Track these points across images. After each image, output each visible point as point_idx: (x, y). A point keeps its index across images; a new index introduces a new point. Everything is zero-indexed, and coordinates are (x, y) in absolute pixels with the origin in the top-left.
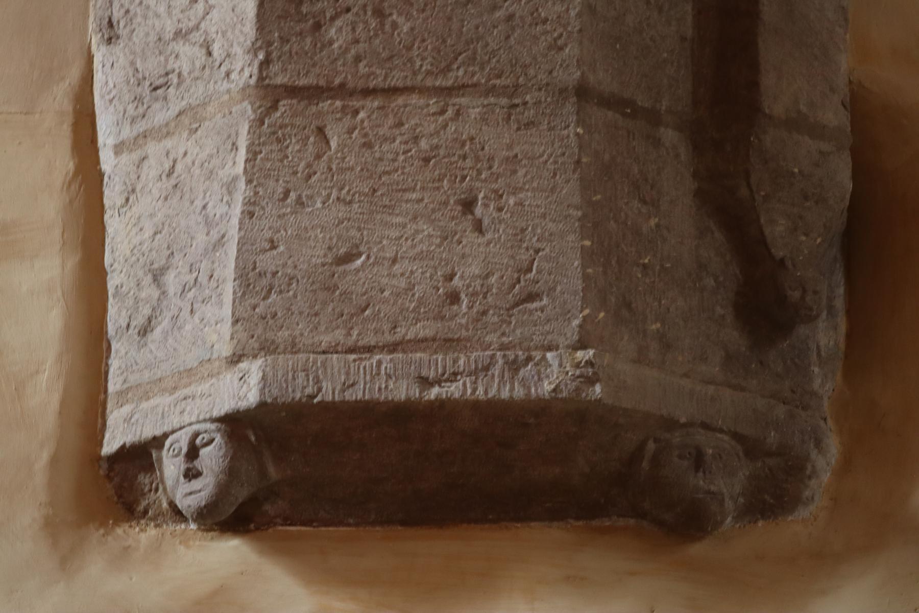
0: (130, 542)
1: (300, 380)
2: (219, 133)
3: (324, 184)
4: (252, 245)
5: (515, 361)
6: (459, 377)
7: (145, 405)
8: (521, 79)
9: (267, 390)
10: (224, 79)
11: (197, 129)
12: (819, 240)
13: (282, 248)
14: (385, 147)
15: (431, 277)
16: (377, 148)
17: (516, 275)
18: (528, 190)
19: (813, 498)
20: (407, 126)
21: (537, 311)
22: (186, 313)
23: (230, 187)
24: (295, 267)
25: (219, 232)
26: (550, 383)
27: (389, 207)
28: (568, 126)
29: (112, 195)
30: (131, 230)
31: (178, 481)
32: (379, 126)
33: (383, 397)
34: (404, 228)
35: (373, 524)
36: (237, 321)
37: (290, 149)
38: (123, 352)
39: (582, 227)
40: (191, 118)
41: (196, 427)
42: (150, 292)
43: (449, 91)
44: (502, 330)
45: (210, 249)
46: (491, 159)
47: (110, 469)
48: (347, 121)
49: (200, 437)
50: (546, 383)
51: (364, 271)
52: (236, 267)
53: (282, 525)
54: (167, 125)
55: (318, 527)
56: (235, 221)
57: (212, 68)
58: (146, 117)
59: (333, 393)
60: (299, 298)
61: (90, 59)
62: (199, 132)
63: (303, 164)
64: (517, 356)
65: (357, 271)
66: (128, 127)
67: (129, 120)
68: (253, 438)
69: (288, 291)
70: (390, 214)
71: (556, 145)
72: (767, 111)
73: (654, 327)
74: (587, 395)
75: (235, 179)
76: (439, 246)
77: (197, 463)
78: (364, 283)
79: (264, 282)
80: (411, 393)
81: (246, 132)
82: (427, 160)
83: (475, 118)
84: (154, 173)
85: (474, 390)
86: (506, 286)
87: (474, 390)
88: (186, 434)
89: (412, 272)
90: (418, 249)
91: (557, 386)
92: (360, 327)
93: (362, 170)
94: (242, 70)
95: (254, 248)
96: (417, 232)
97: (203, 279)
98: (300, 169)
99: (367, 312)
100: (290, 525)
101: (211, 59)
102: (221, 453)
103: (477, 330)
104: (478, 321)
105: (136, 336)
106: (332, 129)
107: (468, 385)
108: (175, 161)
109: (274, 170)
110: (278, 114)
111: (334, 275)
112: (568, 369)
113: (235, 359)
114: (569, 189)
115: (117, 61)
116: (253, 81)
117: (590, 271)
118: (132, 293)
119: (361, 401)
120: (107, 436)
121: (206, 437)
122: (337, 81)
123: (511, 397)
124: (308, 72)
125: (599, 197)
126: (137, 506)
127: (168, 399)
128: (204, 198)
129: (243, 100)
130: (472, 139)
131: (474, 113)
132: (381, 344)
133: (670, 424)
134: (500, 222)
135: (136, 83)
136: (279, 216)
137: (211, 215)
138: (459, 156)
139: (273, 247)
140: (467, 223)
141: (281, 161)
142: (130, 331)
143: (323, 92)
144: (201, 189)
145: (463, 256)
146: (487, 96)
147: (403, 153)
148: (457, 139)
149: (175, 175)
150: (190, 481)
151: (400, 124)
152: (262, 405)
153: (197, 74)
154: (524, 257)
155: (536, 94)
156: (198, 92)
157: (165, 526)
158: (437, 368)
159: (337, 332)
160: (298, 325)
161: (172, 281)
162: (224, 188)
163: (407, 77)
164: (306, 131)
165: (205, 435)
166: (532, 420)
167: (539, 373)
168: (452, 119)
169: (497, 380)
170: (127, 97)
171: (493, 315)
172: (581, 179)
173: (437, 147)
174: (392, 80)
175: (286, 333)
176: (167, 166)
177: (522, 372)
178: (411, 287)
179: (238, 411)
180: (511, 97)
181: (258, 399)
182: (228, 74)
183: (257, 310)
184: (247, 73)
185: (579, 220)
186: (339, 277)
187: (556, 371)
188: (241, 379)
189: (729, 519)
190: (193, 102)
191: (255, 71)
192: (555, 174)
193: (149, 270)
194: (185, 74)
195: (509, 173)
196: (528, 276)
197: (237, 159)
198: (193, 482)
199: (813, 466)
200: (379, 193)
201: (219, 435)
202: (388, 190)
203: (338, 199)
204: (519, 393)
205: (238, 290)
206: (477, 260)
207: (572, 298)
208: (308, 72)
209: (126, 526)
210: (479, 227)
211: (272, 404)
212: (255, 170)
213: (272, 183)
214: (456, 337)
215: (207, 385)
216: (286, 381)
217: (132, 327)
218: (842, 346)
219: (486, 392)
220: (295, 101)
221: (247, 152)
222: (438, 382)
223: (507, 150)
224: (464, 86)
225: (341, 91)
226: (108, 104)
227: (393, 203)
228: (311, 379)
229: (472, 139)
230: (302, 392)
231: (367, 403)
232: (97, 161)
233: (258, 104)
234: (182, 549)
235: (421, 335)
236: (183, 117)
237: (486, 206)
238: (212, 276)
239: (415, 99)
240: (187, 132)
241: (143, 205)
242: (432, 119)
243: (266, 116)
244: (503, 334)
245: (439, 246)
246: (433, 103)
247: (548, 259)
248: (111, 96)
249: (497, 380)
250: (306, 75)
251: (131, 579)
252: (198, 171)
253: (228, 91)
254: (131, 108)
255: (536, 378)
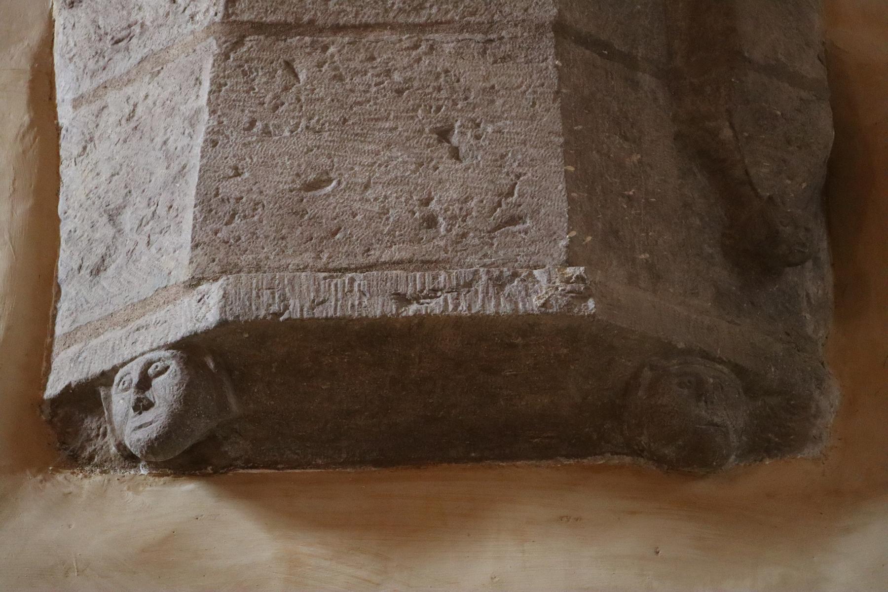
0: (72, 488)
1: (266, 295)
2: (182, 71)
3: (292, 114)
4: (215, 172)
5: (499, 278)
6: (439, 293)
7: (94, 342)
8: (496, 17)
9: (228, 308)
10: (188, 22)
11: (159, 72)
12: (804, 185)
13: (247, 175)
14: (357, 80)
15: (406, 202)
16: (348, 80)
17: (496, 199)
18: (506, 119)
19: (820, 437)
20: (379, 60)
21: (520, 233)
22: (142, 246)
23: (192, 121)
24: (261, 192)
25: (180, 163)
26: (539, 298)
27: (361, 136)
28: (547, 59)
29: (68, 147)
30: (86, 177)
31: (127, 415)
32: (350, 60)
33: (356, 314)
34: (377, 155)
35: (344, 464)
36: (197, 246)
37: (257, 82)
38: (74, 293)
39: (565, 152)
40: (153, 64)
41: (148, 356)
42: (106, 231)
43: (422, 28)
44: (483, 252)
45: (170, 182)
46: (467, 89)
47: (54, 414)
48: (317, 56)
49: (154, 366)
50: (534, 298)
51: (334, 196)
52: (197, 193)
53: (243, 468)
54: (128, 72)
55: (283, 469)
56: (197, 151)
57: (176, 13)
58: (107, 69)
59: (302, 310)
60: (265, 222)
61: (51, 23)
62: (161, 75)
63: (270, 95)
64: (501, 272)
65: (328, 196)
66: (88, 81)
67: (89, 74)
68: (212, 365)
69: (253, 216)
70: (362, 142)
71: (535, 76)
72: (746, 54)
73: (643, 256)
74: (580, 310)
75: (198, 111)
76: (414, 172)
77: (148, 394)
78: (335, 208)
79: (227, 207)
80: (387, 310)
81: (210, 66)
82: (400, 92)
83: (450, 53)
84: (113, 119)
85: (456, 307)
86: (486, 210)
87: (456, 307)
88: (138, 364)
89: (386, 197)
90: (393, 175)
91: (547, 301)
92: (331, 250)
93: (333, 100)
94: (207, 10)
95: (217, 175)
96: (391, 159)
97: (162, 211)
98: (267, 100)
99: (338, 236)
100: (251, 468)
101: (175, 5)
102: (176, 382)
103: (457, 252)
104: (458, 243)
105: (88, 276)
106: (300, 63)
107: (450, 301)
108: (135, 106)
109: (240, 101)
110: (245, 49)
111: (302, 200)
112: (557, 284)
113: (194, 283)
114: (550, 117)
115: (79, 22)
116: (218, 19)
117: (574, 195)
118: (85, 236)
119: (332, 318)
120: (51, 378)
121: (160, 365)
122: (306, 18)
123: (497, 313)
124: (275, 10)
125: (580, 127)
126: (82, 452)
127: (119, 332)
128: (165, 134)
129: (208, 37)
130: (447, 72)
131: (448, 48)
132: (353, 266)
133: (667, 350)
134: (478, 149)
135: (98, 38)
136: (244, 144)
137: (172, 149)
138: (434, 88)
139: (238, 174)
140: (444, 151)
141: (248, 92)
142: (82, 272)
143: (291, 29)
144: (162, 126)
145: (440, 182)
146: (461, 31)
147: (375, 85)
148: (431, 71)
149: (135, 118)
150: (140, 413)
151: (373, 58)
152: (222, 324)
153: (160, 21)
154: (504, 181)
155: (512, 30)
156: (162, 37)
157: (112, 472)
158: (415, 284)
159: (306, 255)
160: (263, 248)
161: (128, 219)
162: (186, 122)
163: (378, 14)
164: (274, 65)
165: (158, 363)
166: (519, 340)
167: (526, 289)
168: (425, 54)
169: (480, 296)
170: (89, 53)
171: (474, 237)
172: (562, 108)
173: (410, 79)
174: (363, 17)
175: (250, 257)
176: (127, 110)
177: (507, 289)
178: (385, 212)
179: (196, 334)
180: (486, 33)
181: (218, 318)
182: (192, 17)
183: (219, 235)
184: (212, 12)
185: (561, 146)
186: (308, 201)
187: (544, 286)
188: (199, 301)
189: (733, 457)
190: (156, 48)
191: (221, 8)
192: (534, 104)
193: (105, 211)
194: (148, 23)
195: (486, 103)
196: (510, 200)
197: (200, 93)
198: (145, 413)
199: (818, 407)
200: (350, 122)
201: (174, 362)
202: (360, 120)
203: (307, 127)
204: (506, 308)
205: (198, 215)
206: (453, 185)
207: (558, 219)
208: (275, 10)
209: (68, 473)
210: (455, 154)
211: (234, 321)
212: (219, 101)
213: (237, 113)
214: (434, 258)
215: (163, 312)
216: (249, 299)
217: (84, 269)
218: (831, 296)
219: (469, 308)
220: (262, 37)
221: (211, 85)
222: (417, 299)
223: (484, 81)
224: (438, 23)
225: (311, 27)
226: (68, 61)
227: (365, 131)
228: (277, 296)
229: (447, 72)
230: (267, 310)
231: (339, 319)
232: (55, 117)
233: (223, 39)
234: (130, 495)
235: (397, 257)
236: (145, 63)
237: (463, 134)
238: (171, 207)
239: (387, 35)
240: (149, 76)
241: (100, 151)
242: (405, 53)
243: (231, 50)
244: (485, 256)
245: (414, 172)
246: (406, 40)
247: (530, 183)
248: (72, 54)
249: (480, 296)
250: (274, 12)
251: (70, 527)
252: (159, 110)
253: (193, 32)
254: (91, 65)
255: (523, 293)
